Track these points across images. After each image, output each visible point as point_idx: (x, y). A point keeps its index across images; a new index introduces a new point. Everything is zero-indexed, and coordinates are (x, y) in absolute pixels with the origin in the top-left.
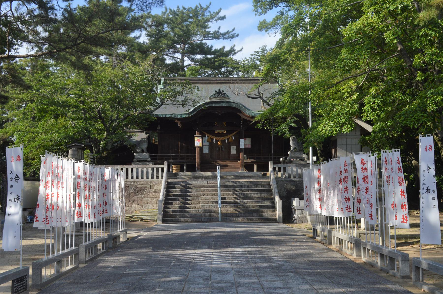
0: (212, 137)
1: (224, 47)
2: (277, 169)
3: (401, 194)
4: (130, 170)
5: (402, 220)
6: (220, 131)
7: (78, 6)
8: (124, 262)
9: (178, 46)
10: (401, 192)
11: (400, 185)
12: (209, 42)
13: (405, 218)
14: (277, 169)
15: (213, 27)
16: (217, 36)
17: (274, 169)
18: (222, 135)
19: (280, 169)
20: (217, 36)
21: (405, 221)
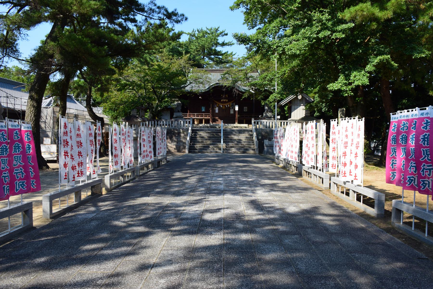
0: (224, 104)
1: (228, 52)
2: (256, 122)
3: (65, 155)
4: (283, 123)
5: (65, 177)
6: (224, 100)
7: (244, 24)
8: (24, 261)
9: (144, 42)
10: (65, 153)
11: (64, 147)
12: (219, 49)
13: (80, 172)
14: (256, 122)
15: (221, 40)
16: (223, 44)
17: (255, 122)
18: (225, 102)
19: (258, 123)
20: (223, 44)
21: (80, 175)
